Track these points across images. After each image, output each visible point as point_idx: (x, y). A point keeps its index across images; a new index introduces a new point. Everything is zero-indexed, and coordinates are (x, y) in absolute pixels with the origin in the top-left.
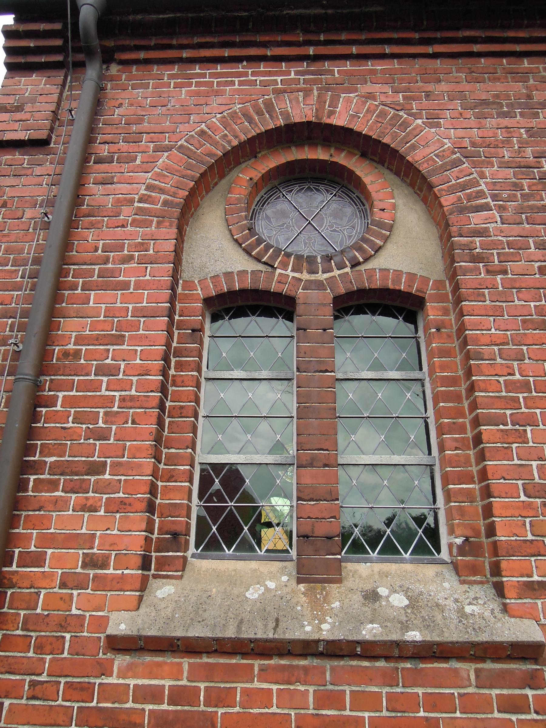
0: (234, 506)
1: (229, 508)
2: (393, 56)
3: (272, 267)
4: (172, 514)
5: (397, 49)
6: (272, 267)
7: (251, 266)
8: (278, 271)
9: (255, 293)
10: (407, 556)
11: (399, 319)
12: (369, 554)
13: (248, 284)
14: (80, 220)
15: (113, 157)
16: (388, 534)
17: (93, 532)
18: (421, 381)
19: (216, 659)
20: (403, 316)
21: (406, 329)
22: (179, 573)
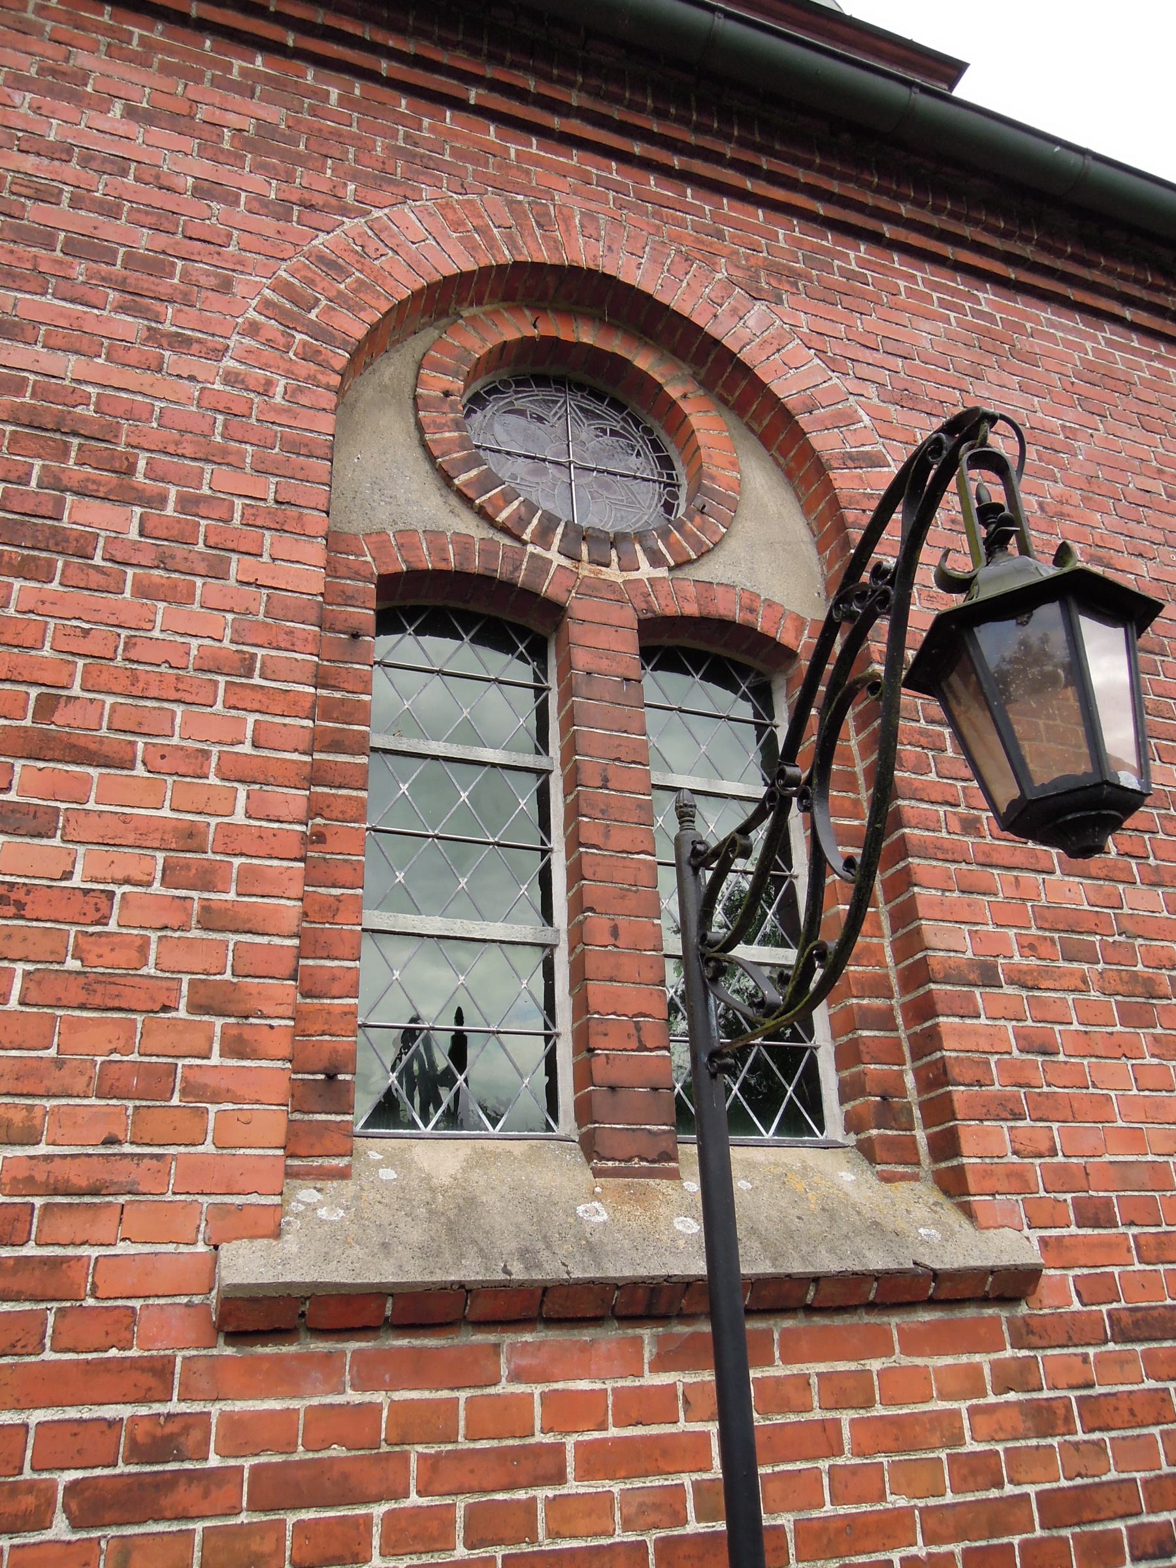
0: (765, 1047)
1: (755, 1050)
2: (1134, 327)
3: (518, 538)
4: (334, 1029)
5: (1144, 318)
6: (518, 538)
7: (468, 525)
8: (530, 548)
9: (483, 583)
10: (769, 1136)
11: (462, 639)
12: (761, 1134)
13: (476, 565)
14: (1011, 533)
15: (120, 207)
16: (791, 1097)
17: (170, 1060)
18: (543, 774)
19: (831, 1364)
20: (527, 642)
21: (523, 672)
22: (341, 1162)
